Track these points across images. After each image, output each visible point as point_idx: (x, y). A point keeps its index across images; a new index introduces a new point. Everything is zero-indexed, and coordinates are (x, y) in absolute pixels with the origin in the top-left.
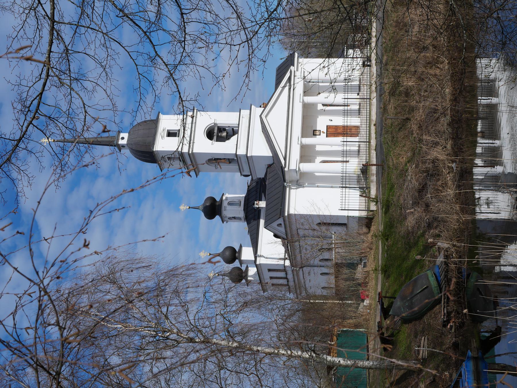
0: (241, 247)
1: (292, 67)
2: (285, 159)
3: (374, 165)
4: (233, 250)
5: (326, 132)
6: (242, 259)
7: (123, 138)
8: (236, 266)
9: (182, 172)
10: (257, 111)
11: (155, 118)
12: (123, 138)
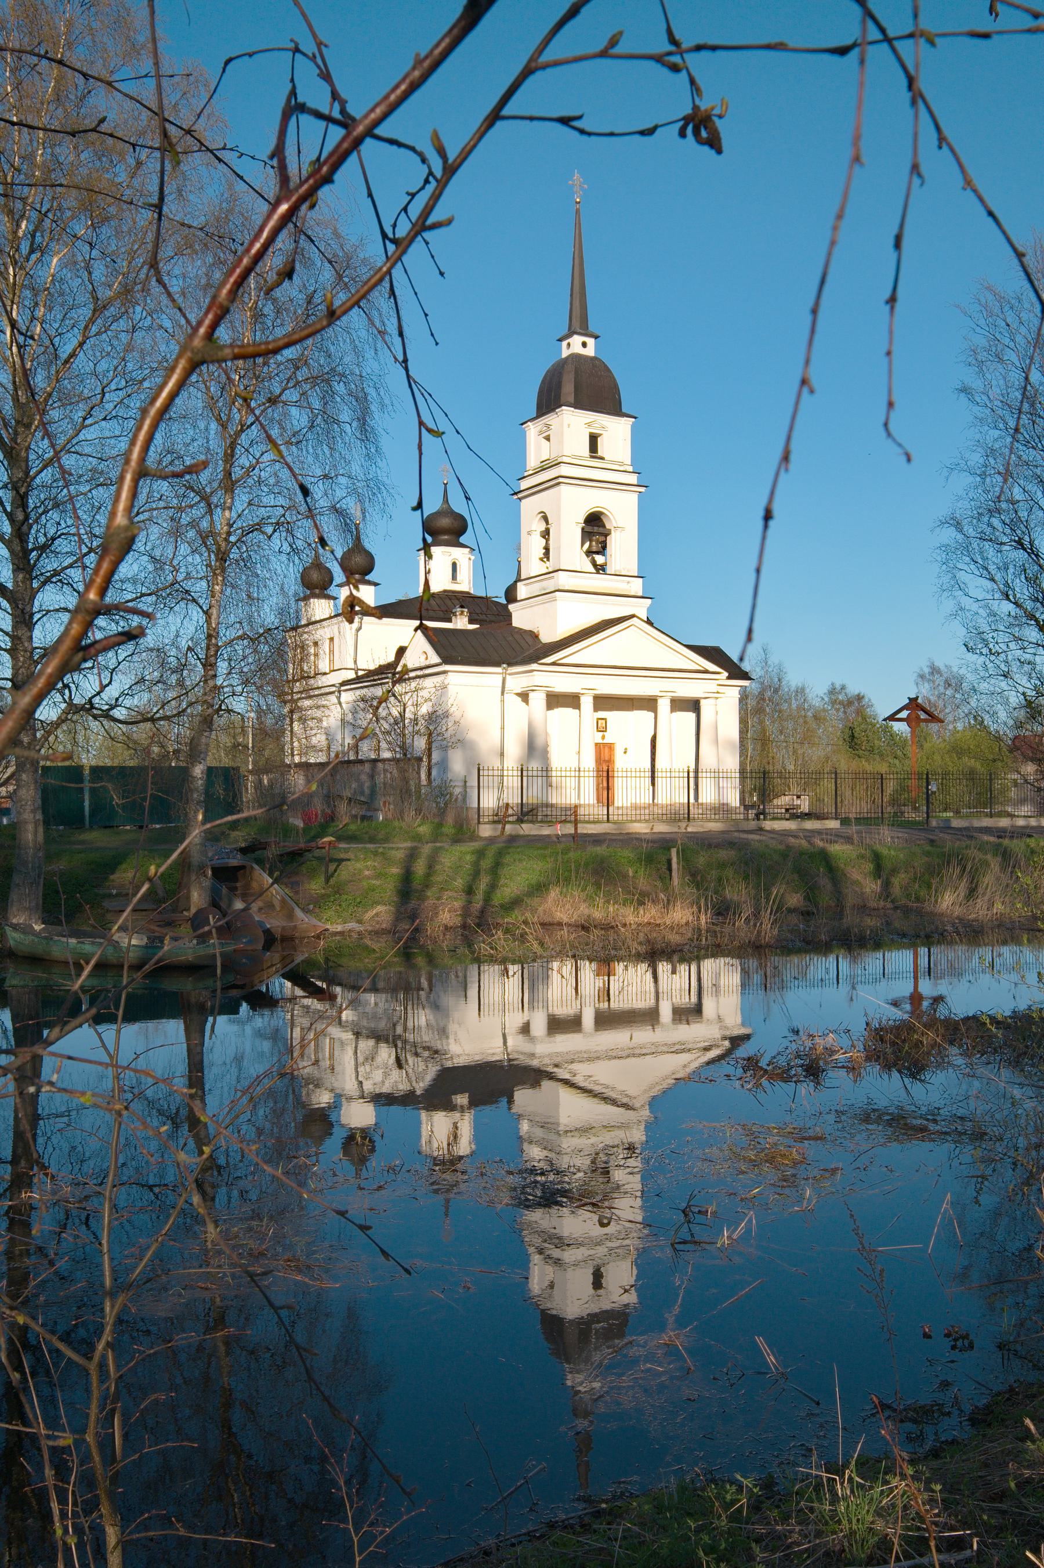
0: (376, 584)
1: (726, 674)
2: (554, 664)
3: (576, 829)
4: (369, 569)
5: (605, 741)
6: (312, 600)
7: (584, 345)
8: (335, 575)
9: (171, 608)
10: (641, 608)
11: (624, 410)
12: (584, 345)
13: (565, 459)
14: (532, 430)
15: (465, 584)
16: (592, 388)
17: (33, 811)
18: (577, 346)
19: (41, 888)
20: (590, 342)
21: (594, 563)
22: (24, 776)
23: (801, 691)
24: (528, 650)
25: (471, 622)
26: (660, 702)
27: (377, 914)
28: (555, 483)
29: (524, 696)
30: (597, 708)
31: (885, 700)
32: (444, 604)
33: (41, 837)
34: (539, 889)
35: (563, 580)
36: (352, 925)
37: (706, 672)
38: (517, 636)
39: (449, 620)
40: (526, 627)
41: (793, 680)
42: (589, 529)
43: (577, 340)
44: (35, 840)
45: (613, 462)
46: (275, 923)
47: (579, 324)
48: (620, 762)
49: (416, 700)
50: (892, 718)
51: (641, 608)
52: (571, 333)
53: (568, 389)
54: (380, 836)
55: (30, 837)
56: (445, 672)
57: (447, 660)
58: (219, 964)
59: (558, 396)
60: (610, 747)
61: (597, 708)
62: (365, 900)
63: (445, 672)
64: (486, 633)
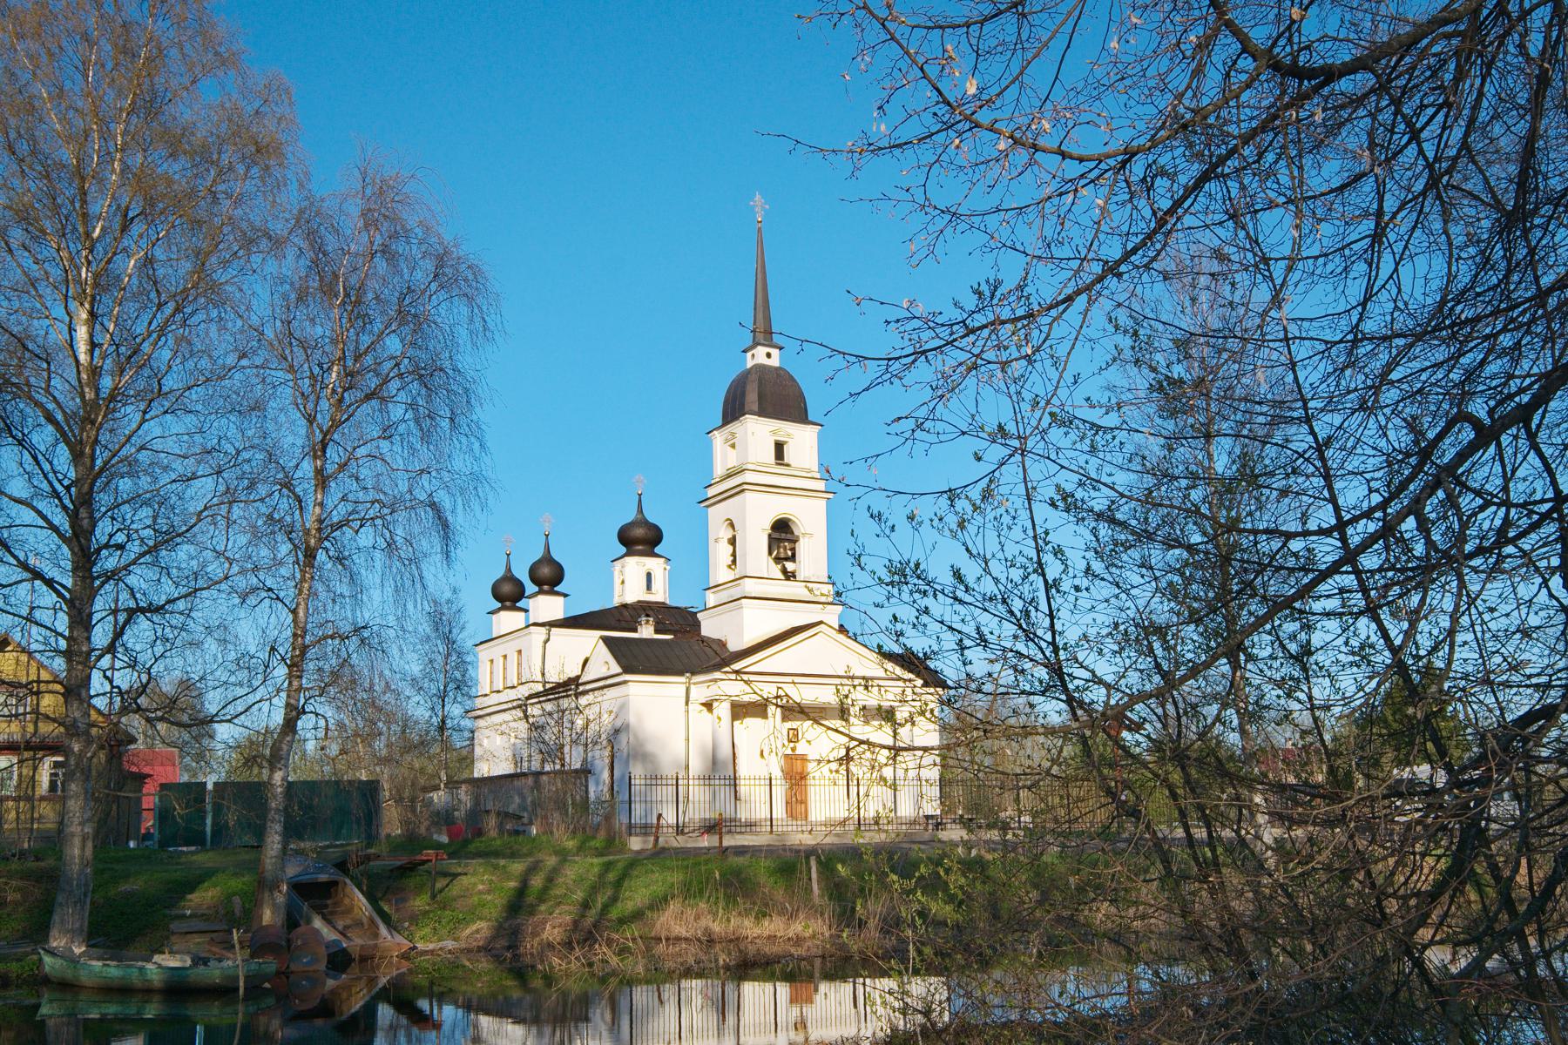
0: (566, 596)
7: (769, 355)
12: (769, 355)
13: (750, 467)
14: (718, 438)
15: (659, 595)
16: (779, 398)
17: (82, 824)
18: (760, 356)
19: (88, 907)
20: (775, 352)
21: (784, 571)
22: (73, 786)
24: (716, 658)
25: (657, 631)
27: (477, 931)
28: (739, 490)
29: (708, 706)
30: (785, 719)
32: (625, 616)
33: (89, 851)
34: (659, 903)
35: (750, 587)
36: (450, 944)
38: (715, 647)
39: (635, 630)
40: (715, 636)
42: (776, 535)
43: (761, 351)
44: (82, 857)
45: (797, 469)
46: (356, 943)
47: (764, 334)
49: (597, 710)
51: (832, 615)
52: (755, 344)
53: (752, 397)
54: (525, 850)
55: (77, 852)
56: (625, 682)
57: (628, 669)
58: (241, 984)
59: (742, 405)
61: (785, 719)
62: (473, 914)
63: (625, 682)
64: (669, 642)
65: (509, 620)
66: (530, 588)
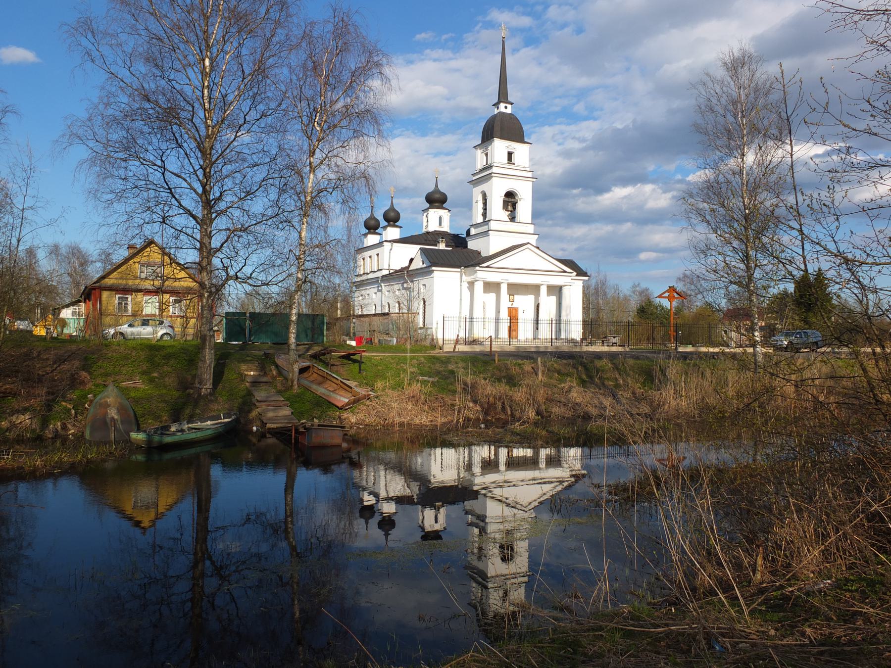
0: (400, 227)
1: (575, 274)
2: (487, 267)
7: (506, 107)
12: (506, 107)
15: (446, 228)
20: (509, 106)
23: (616, 288)
24: (474, 260)
26: (542, 287)
31: (657, 290)
37: (565, 272)
41: (611, 281)
45: (518, 166)
48: (520, 316)
50: (660, 296)
53: (497, 128)
60: (516, 309)
64: (457, 251)
65: (372, 239)
66: (383, 223)
